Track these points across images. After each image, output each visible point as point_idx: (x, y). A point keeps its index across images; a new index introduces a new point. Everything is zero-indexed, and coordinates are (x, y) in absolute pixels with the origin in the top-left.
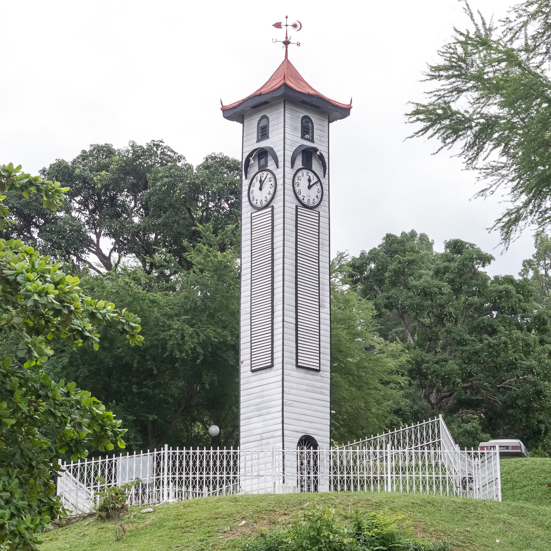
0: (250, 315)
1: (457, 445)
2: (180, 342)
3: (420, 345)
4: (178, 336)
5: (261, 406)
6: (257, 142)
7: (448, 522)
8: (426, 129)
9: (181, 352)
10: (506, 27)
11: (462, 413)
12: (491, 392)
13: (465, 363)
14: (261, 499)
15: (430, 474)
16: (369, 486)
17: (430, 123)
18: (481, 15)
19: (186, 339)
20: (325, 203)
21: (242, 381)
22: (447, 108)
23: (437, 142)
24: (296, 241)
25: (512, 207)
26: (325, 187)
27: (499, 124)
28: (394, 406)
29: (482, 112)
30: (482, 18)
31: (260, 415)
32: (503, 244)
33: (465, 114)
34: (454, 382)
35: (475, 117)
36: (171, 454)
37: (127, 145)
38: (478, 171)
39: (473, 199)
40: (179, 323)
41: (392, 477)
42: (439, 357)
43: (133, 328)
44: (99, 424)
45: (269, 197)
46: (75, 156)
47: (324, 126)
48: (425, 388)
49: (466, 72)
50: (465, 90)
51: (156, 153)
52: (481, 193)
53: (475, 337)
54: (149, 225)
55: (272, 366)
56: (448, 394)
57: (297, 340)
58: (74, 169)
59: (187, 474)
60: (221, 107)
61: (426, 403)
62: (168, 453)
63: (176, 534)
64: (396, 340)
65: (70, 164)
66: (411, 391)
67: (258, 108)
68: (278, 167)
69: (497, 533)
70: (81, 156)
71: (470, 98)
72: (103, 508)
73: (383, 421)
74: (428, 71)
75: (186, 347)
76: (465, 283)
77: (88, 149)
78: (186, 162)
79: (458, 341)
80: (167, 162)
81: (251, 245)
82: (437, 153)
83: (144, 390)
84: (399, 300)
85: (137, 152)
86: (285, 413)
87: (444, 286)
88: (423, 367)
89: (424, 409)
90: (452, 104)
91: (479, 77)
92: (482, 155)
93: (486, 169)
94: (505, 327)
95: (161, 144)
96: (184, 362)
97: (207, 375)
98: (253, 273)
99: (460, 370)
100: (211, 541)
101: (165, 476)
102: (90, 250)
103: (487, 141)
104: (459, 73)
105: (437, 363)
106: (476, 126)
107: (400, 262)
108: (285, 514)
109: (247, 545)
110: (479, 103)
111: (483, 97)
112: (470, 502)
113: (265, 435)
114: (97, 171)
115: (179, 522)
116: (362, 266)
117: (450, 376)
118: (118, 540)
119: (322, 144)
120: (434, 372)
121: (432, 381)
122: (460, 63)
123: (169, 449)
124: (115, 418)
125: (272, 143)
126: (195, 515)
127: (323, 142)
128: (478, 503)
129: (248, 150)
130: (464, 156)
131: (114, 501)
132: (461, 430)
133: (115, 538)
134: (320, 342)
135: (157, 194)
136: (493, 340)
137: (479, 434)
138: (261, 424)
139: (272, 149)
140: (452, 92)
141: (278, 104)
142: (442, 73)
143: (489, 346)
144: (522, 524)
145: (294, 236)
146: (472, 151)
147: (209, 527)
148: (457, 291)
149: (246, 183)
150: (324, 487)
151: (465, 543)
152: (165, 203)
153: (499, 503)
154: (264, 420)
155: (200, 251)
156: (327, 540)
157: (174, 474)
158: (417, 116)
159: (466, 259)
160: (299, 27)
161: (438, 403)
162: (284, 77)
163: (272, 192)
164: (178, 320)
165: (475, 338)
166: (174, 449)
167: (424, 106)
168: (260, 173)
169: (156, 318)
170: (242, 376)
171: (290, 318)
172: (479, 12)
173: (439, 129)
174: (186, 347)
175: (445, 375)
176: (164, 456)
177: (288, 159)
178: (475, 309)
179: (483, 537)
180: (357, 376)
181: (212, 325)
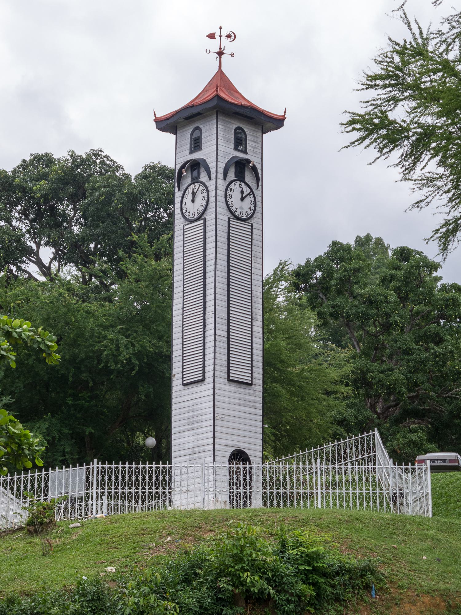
0: (181, 328)
1: (392, 459)
2: (115, 353)
3: (365, 354)
4: (113, 347)
5: (193, 420)
6: (191, 152)
7: (375, 538)
8: (363, 139)
9: (116, 363)
10: (439, 39)
11: (408, 423)
12: (437, 402)
13: (411, 372)
14: (188, 515)
15: (361, 489)
16: (298, 502)
17: (366, 133)
18: (418, 24)
19: (121, 349)
20: (258, 215)
21: (174, 395)
22: (383, 117)
23: (373, 152)
24: (229, 254)
25: (450, 217)
26: (258, 199)
27: (437, 134)
28: (338, 416)
29: (420, 121)
30: (419, 28)
31: (192, 429)
32: (441, 255)
33: (402, 123)
34: (399, 392)
35: (412, 127)
36: (100, 468)
37: (66, 155)
38: (413, 182)
39: (408, 211)
40: (113, 333)
41: (322, 493)
42: (386, 366)
43: (49, 347)
44: (16, 443)
45: (201, 209)
46: (15, 165)
47: (257, 137)
48: (371, 397)
49: (403, 81)
50: (402, 100)
51: (95, 162)
52: (417, 205)
53: (422, 346)
54: (87, 236)
55: (203, 380)
56: (394, 403)
57: (229, 354)
58: (14, 178)
59: (116, 489)
60: (154, 118)
61: (371, 413)
62: (98, 468)
63: (102, 550)
64: (348, 347)
65: (10, 174)
66: (356, 401)
67: (191, 119)
68: (210, 179)
69: (424, 550)
70: (22, 165)
71: (406, 107)
72: (31, 523)
73: (326, 431)
74: (364, 80)
75: (121, 358)
76: (411, 291)
77: (28, 158)
78: (124, 172)
79: (403, 350)
80: (107, 171)
81: (184, 257)
82: (373, 162)
83: (80, 402)
84: (344, 309)
85: (76, 161)
86: (216, 428)
87: (390, 295)
88: (368, 376)
89: (368, 419)
90: (389, 114)
91: (416, 87)
92: (420, 165)
93: (421, 180)
94: (451, 336)
95: (100, 153)
96: (120, 373)
97: (143, 386)
98: (185, 286)
99: (406, 380)
100: (136, 557)
101: (94, 491)
102: (30, 260)
103: (424, 151)
104: (396, 82)
105: (382, 372)
106: (413, 136)
107: (345, 270)
108: (210, 531)
109: (170, 562)
110: (417, 112)
111: (420, 107)
112: (399, 519)
113: (196, 450)
114: (37, 181)
115: (106, 538)
116: (308, 274)
117: (396, 386)
118: (44, 555)
119: (255, 155)
120: (379, 381)
121: (377, 391)
122: (397, 72)
123: (98, 464)
124: (32, 437)
125: (205, 155)
126: (121, 531)
127: (256, 154)
128: (406, 519)
129: (181, 161)
130: (401, 166)
131: (42, 516)
132: (407, 440)
133: (41, 553)
134: (252, 355)
135: (95, 203)
136: (439, 350)
137: (424, 444)
138: (193, 438)
139: (204, 161)
140: (389, 101)
141: (211, 115)
142: (378, 82)
143: (435, 355)
144: (451, 540)
145: (227, 248)
146: (410, 161)
147: (134, 543)
148: (403, 299)
149: (178, 195)
150: (257, 503)
151: (391, 560)
152: (103, 213)
153: (429, 519)
154: (196, 434)
155: (135, 261)
156: (250, 558)
157: (103, 489)
158: (353, 126)
159: (412, 267)
160: (233, 38)
161: (384, 413)
162: (217, 88)
163: (204, 204)
164: (113, 331)
165: (421, 348)
166: (103, 463)
167: (360, 116)
168: (193, 185)
169: (91, 329)
170: (174, 389)
171: (222, 332)
172: (416, 21)
173: (376, 139)
174: (121, 358)
175: (390, 385)
176: (93, 471)
177: (221, 170)
178: (423, 317)
179: (410, 554)
180: (298, 386)
181: (148, 336)
